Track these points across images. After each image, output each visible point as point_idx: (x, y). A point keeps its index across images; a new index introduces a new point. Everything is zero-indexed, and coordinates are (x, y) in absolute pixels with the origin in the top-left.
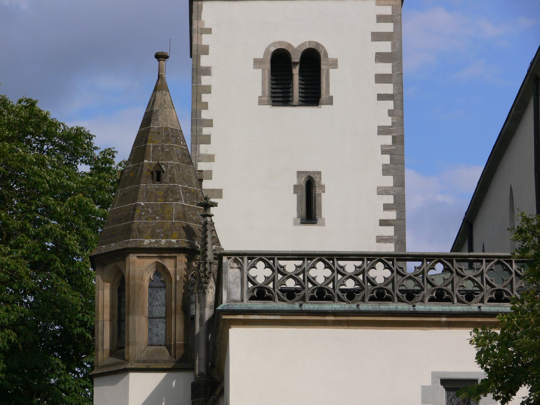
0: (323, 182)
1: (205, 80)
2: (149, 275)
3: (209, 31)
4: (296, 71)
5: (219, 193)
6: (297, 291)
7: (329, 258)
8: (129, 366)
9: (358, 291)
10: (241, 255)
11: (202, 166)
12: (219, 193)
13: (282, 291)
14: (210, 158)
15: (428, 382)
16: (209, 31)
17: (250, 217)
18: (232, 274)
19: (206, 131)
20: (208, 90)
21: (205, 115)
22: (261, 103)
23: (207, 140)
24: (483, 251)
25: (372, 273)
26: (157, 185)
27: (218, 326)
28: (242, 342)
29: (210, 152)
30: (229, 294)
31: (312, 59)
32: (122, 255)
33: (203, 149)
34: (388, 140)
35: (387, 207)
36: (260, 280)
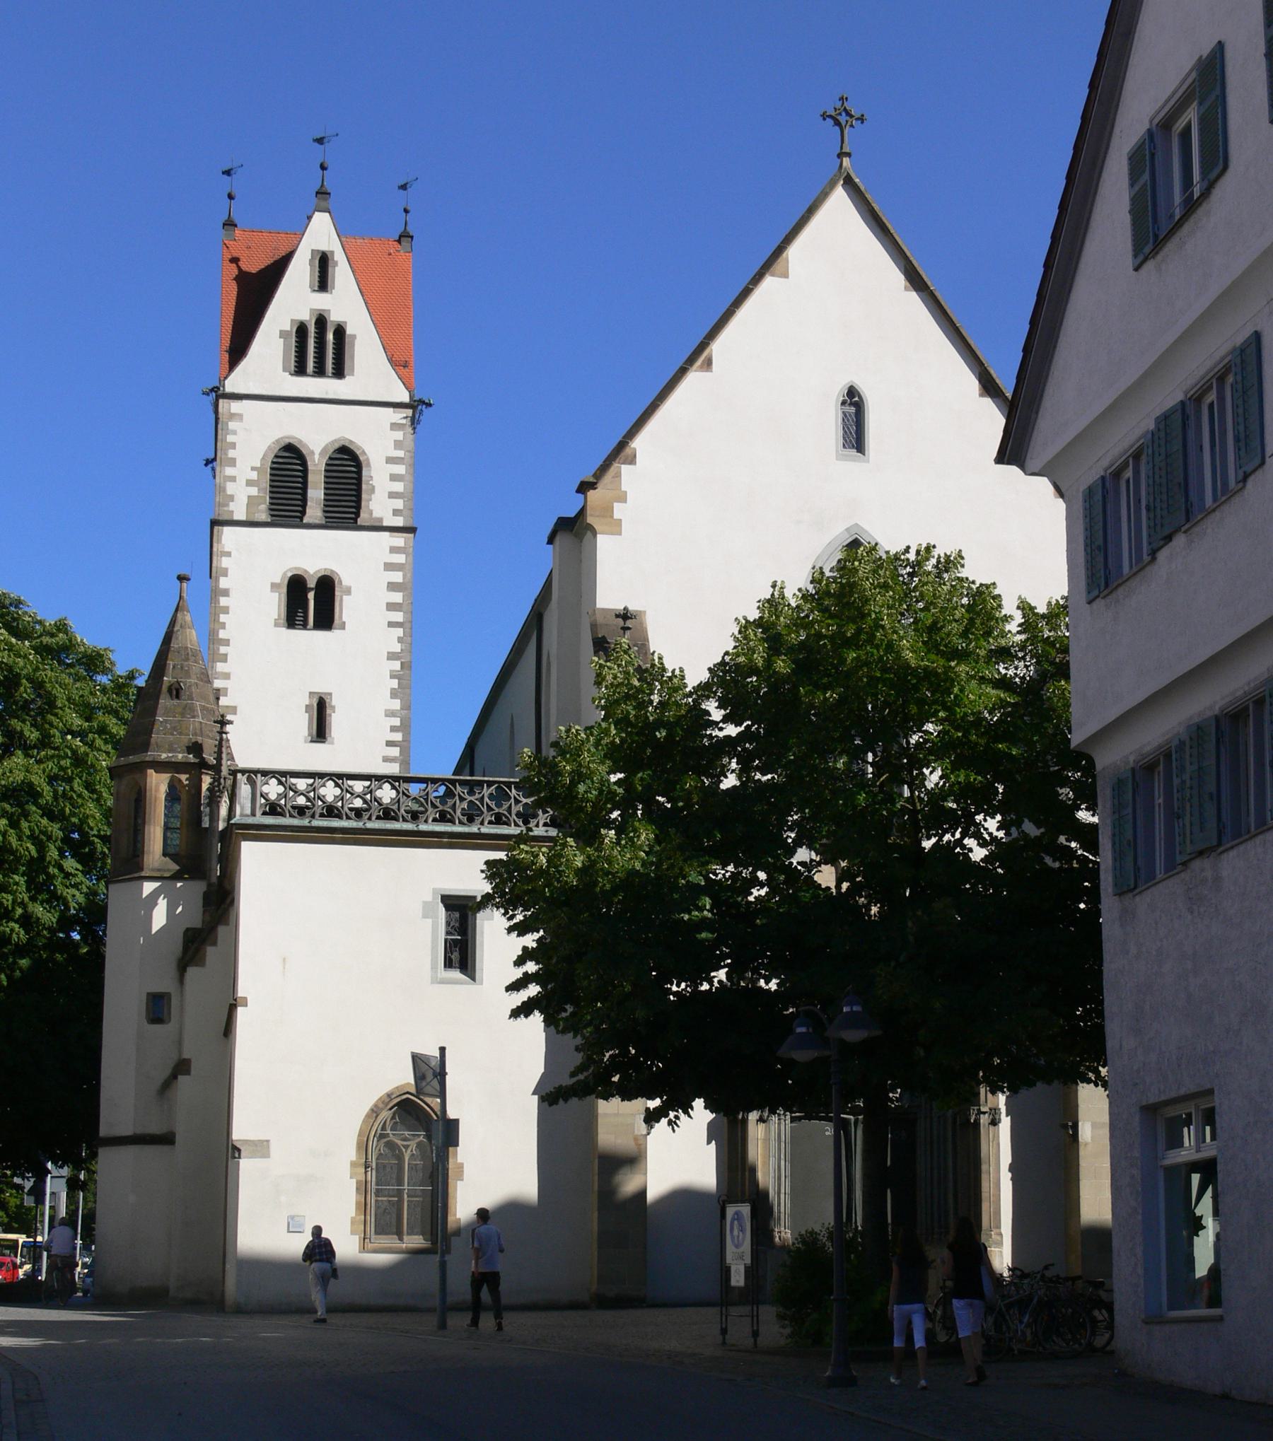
0: (333, 703)
1: (223, 601)
2: (163, 788)
3: (229, 554)
4: (311, 596)
5: (234, 710)
6: (307, 807)
7: (339, 778)
8: (143, 874)
9: (366, 810)
10: (256, 772)
11: (217, 684)
12: (234, 710)
13: (294, 807)
14: (227, 676)
15: (429, 898)
16: (229, 554)
17: (263, 734)
18: (244, 790)
19: (223, 650)
20: (226, 610)
21: (222, 634)
22: (276, 625)
23: (224, 658)
24: (472, 774)
25: (379, 793)
26: (176, 702)
27: (233, 835)
28: (251, 853)
29: (226, 671)
30: (242, 808)
31: (327, 586)
32: (142, 767)
33: (220, 667)
34: (396, 665)
35: (393, 729)
36: (386, 800)
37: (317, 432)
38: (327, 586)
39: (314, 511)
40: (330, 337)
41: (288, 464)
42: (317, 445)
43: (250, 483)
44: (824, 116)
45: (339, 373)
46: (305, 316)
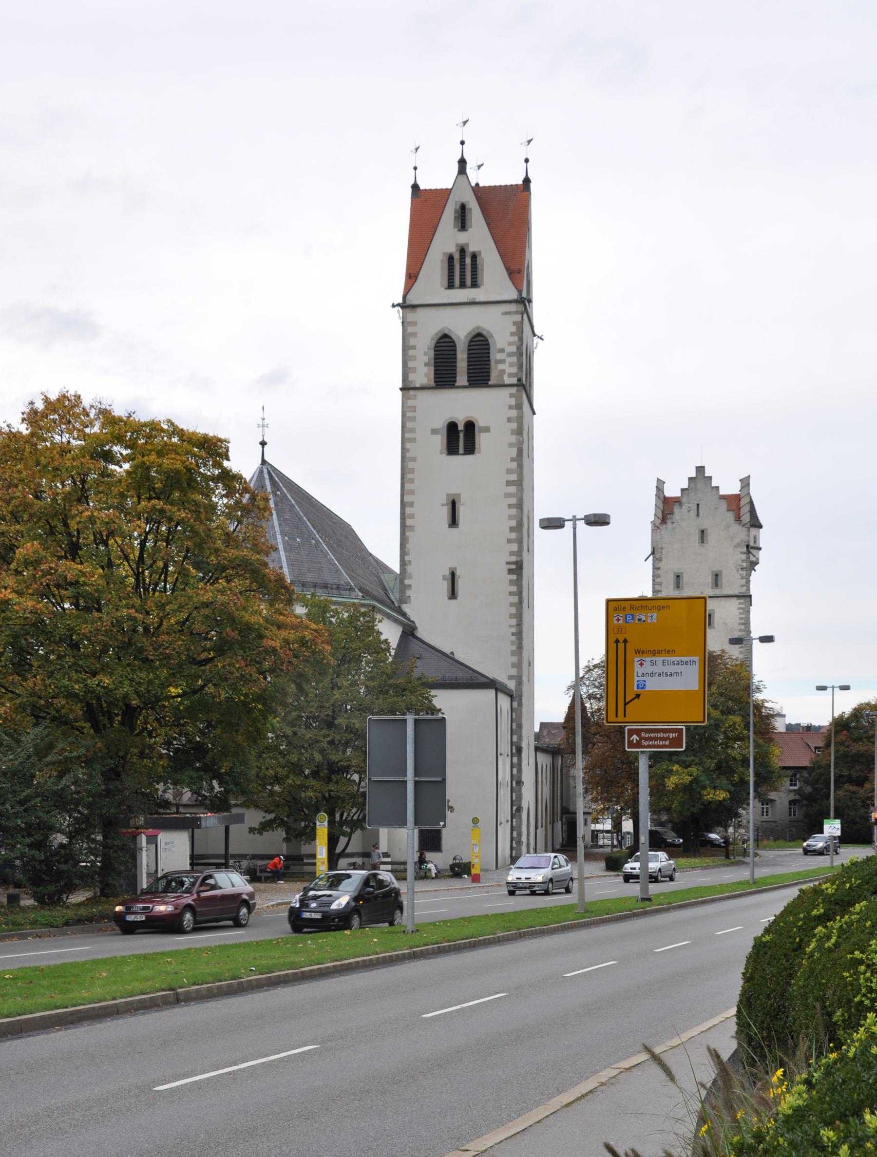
4: (461, 435)
37: (461, 325)
40: (468, 261)
42: (461, 333)
43: (425, 354)
45: (475, 285)
46: (452, 249)
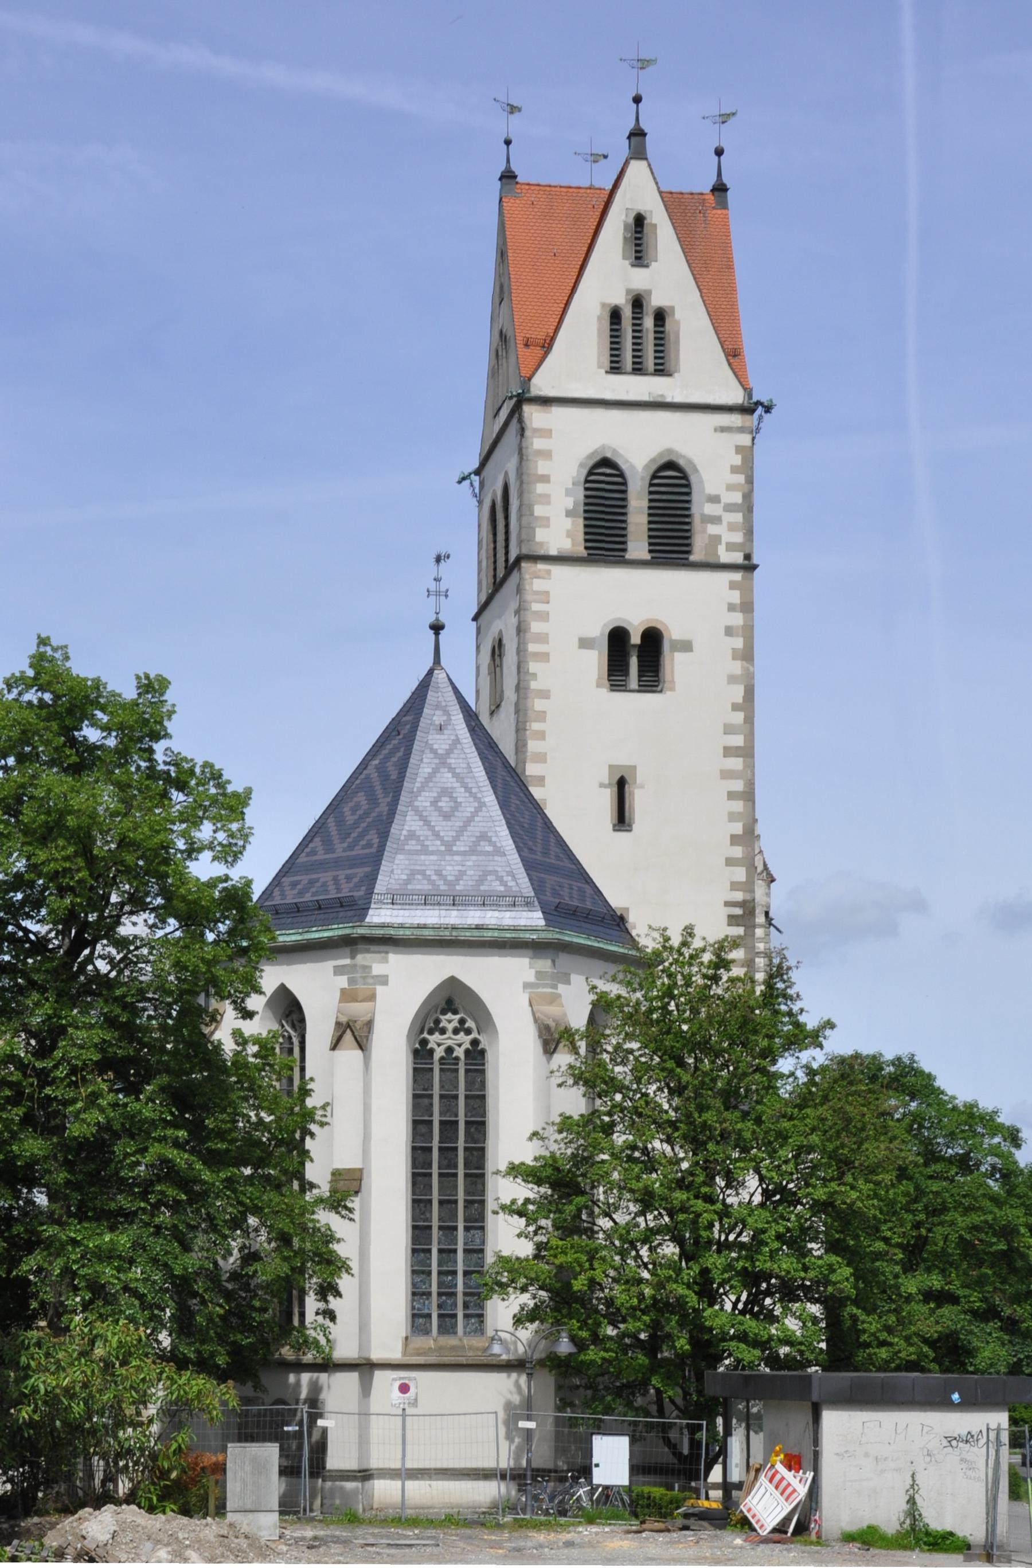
37: (638, 444)
38: (653, 639)
39: (638, 547)
40: (649, 323)
41: (604, 480)
44: (519, 1236)
45: (661, 370)
46: (620, 299)
